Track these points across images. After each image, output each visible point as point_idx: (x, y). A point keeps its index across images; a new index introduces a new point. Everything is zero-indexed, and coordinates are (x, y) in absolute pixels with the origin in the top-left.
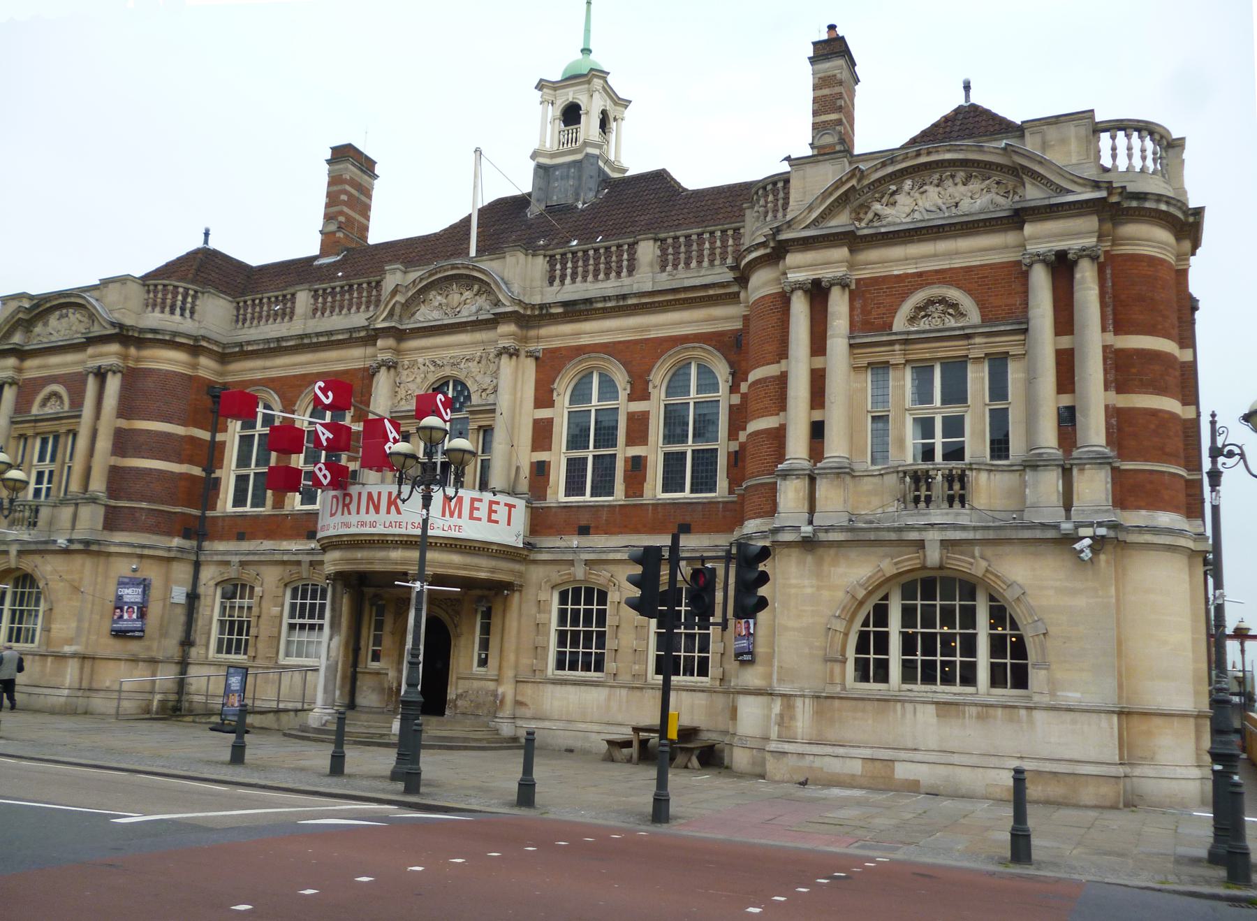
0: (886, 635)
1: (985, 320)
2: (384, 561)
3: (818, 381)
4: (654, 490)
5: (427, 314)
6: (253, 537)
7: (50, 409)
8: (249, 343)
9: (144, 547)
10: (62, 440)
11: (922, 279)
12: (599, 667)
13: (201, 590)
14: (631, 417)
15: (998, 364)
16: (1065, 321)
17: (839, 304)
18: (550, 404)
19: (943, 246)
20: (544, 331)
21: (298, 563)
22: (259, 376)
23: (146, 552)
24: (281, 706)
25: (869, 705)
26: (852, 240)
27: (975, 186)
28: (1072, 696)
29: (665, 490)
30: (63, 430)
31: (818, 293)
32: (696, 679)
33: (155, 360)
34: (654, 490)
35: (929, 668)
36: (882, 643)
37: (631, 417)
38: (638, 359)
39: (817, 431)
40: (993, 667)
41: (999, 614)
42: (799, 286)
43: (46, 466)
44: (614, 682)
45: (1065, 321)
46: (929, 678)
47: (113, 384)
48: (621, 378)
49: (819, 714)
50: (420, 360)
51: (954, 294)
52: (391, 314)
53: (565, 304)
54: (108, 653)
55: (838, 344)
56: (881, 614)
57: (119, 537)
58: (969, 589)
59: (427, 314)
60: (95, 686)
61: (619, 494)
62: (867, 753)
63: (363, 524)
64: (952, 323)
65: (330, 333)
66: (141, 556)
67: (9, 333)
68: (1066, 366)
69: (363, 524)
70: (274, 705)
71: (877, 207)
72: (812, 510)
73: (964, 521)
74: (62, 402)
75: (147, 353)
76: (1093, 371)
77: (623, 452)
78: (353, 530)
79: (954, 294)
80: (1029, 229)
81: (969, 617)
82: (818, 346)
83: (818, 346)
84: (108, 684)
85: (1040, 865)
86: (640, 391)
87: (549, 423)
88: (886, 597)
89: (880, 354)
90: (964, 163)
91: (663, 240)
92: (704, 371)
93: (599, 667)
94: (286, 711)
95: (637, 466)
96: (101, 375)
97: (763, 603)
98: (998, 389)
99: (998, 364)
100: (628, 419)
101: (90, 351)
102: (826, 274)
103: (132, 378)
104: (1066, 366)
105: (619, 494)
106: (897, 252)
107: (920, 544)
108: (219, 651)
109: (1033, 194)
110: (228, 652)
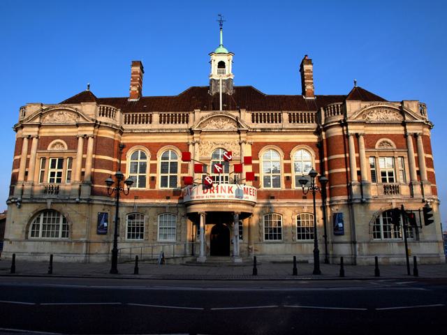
0: (379, 226)
1: (397, 148)
2: (227, 208)
3: (28, 160)
4: (159, 187)
5: (209, 127)
6: (142, 198)
7: (56, 149)
8: (135, 130)
9: (106, 201)
10: (47, 161)
11: (381, 136)
12: (280, 238)
13: (120, 216)
14: (151, 165)
15: (71, 159)
16: (85, 151)
17: (35, 141)
18: (156, 159)
19: (390, 128)
20: (253, 137)
21: (164, 207)
22: (139, 141)
23: (107, 203)
24: (175, 256)
25: (382, 244)
26: (40, 126)
27: (391, 114)
28: (428, 239)
29: (161, 186)
30: (66, 157)
31: (30, 138)
32: (139, 239)
33: (101, 133)
34: (159, 187)
35: (133, 235)
36: (378, 228)
37: (151, 165)
38: (154, 148)
39: (26, 173)
40: (63, 232)
41: (65, 220)
42: (352, 134)
43: (56, 170)
44: (285, 242)
45: (85, 151)
46: (133, 237)
47: (91, 141)
48: (148, 154)
49: (369, 247)
50: (209, 142)
51: (389, 140)
52: (199, 126)
53: (261, 129)
54: (96, 240)
55: (33, 151)
56: (378, 221)
57: (96, 198)
58: (59, 214)
59: (209, 127)
60: (91, 252)
61: (148, 188)
62: (383, 256)
63: (220, 196)
64: (389, 148)
65: (172, 130)
66: (105, 205)
67: (35, 118)
68: (84, 161)
69: (220, 196)
70: (172, 256)
71: (368, 116)
72: (80, 195)
73: (400, 197)
74: (63, 147)
75: (100, 131)
76: (89, 164)
77: (148, 175)
78: (216, 198)
79: (389, 140)
80: (24, 129)
81: (58, 219)
82: (29, 152)
83: (358, 150)
84: (97, 251)
85: (120, 274)
86: (154, 158)
87: (156, 165)
88: (379, 216)
89: (373, 154)
90: (389, 108)
91: (290, 114)
92: (173, 153)
93: (280, 238)
94: (177, 257)
95: (153, 179)
96: (86, 138)
97: (432, 221)
98: (70, 166)
99: (71, 159)
100: (162, 166)
101: (79, 128)
102: (359, 132)
103: (97, 139)
104: (84, 161)
105: (148, 188)
106: (374, 128)
107: (46, 203)
108: (43, 236)
109: (81, 120)
110: (53, 237)
